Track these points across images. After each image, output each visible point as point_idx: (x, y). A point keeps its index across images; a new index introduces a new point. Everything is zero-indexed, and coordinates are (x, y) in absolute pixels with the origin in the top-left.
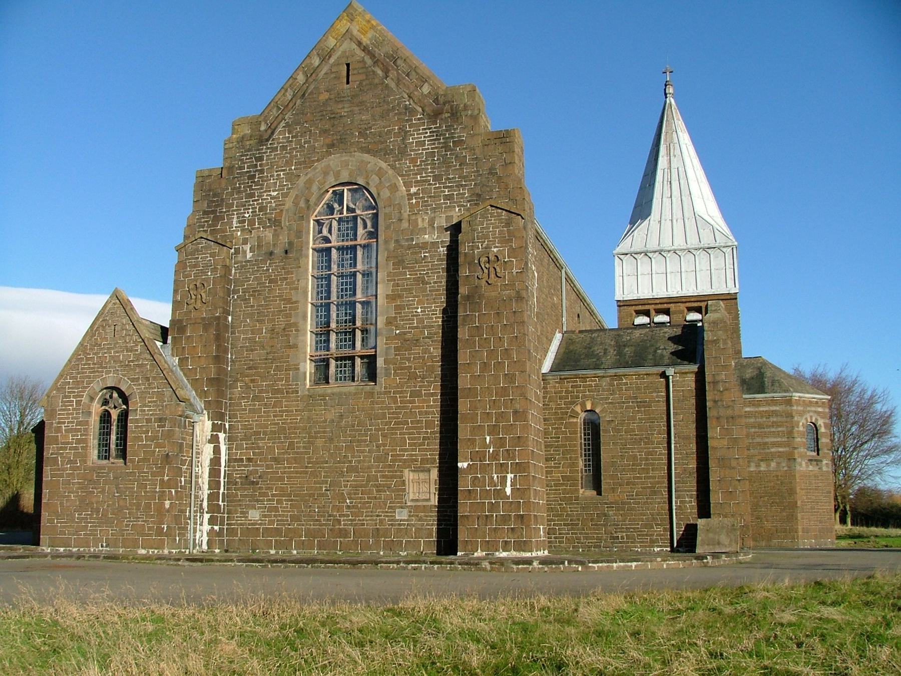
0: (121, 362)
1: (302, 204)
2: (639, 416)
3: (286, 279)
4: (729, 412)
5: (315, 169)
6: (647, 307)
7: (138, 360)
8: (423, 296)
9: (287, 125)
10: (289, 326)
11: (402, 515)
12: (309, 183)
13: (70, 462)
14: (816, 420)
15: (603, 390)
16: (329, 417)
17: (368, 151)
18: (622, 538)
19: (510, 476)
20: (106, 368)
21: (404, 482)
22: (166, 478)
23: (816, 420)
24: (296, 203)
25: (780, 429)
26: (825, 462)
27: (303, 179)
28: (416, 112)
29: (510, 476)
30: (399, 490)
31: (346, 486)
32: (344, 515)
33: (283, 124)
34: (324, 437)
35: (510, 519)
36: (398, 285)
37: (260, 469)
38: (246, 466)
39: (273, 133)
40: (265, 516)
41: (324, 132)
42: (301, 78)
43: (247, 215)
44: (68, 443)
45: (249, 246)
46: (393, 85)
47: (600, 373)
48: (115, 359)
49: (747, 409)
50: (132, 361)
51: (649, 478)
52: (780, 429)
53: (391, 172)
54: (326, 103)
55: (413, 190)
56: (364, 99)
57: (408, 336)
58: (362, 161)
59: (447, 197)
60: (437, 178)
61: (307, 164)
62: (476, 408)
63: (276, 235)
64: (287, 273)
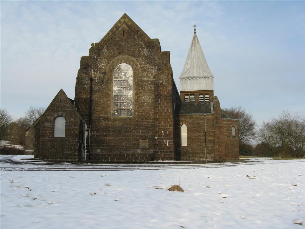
0: (63, 109)
1: (111, 68)
2: (197, 126)
3: (107, 88)
4: (220, 125)
5: (115, 59)
6: (188, 93)
7: (68, 109)
8: (145, 94)
9: (107, 46)
10: (108, 101)
11: (139, 151)
12: (113, 63)
13: (48, 136)
14: (235, 126)
15: (188, 119)
16: (119, 125)
17: (130, 55)
18: (192, 157)
19: (168, 141)
20: (58, 111)
21: (139, 142)
22: (76, 141)
23: (235, 126)
24: (110, 67)
25: (225, 128)
26: (237, 137)
27: (111, 62)
28: (143, 46)
29: (168, 141)
30: (138, 144)
31: (124, 143)
32: (123, 151)
33: (106, 46)
34: (118, 130)
35: (168, 152)
36: (138, 91)
37: (100, 139)
38: (96, 137)
39: (103, 48)
40: (101, 151)
41: (117, 49)
42: (111, 33)
43: (96, 70)
44: (47, 131)
45: (96, 78)
46: (136, 38)
47: (187, 114)
48: (62, 109)
49: (233, 129)
50: (66, 109)
51: (200, 141)
52: (225, 128)
53: (136, 61)
54: (118, 41)
55: (142, 66)
56: (129, 41)
57: (141, 104)
58: (128, 58)
59: (151, 69)
60: (148, 63)
61: (113, 57)
62: (159, 124)
63: (104, 76)
64: (108, 86)
